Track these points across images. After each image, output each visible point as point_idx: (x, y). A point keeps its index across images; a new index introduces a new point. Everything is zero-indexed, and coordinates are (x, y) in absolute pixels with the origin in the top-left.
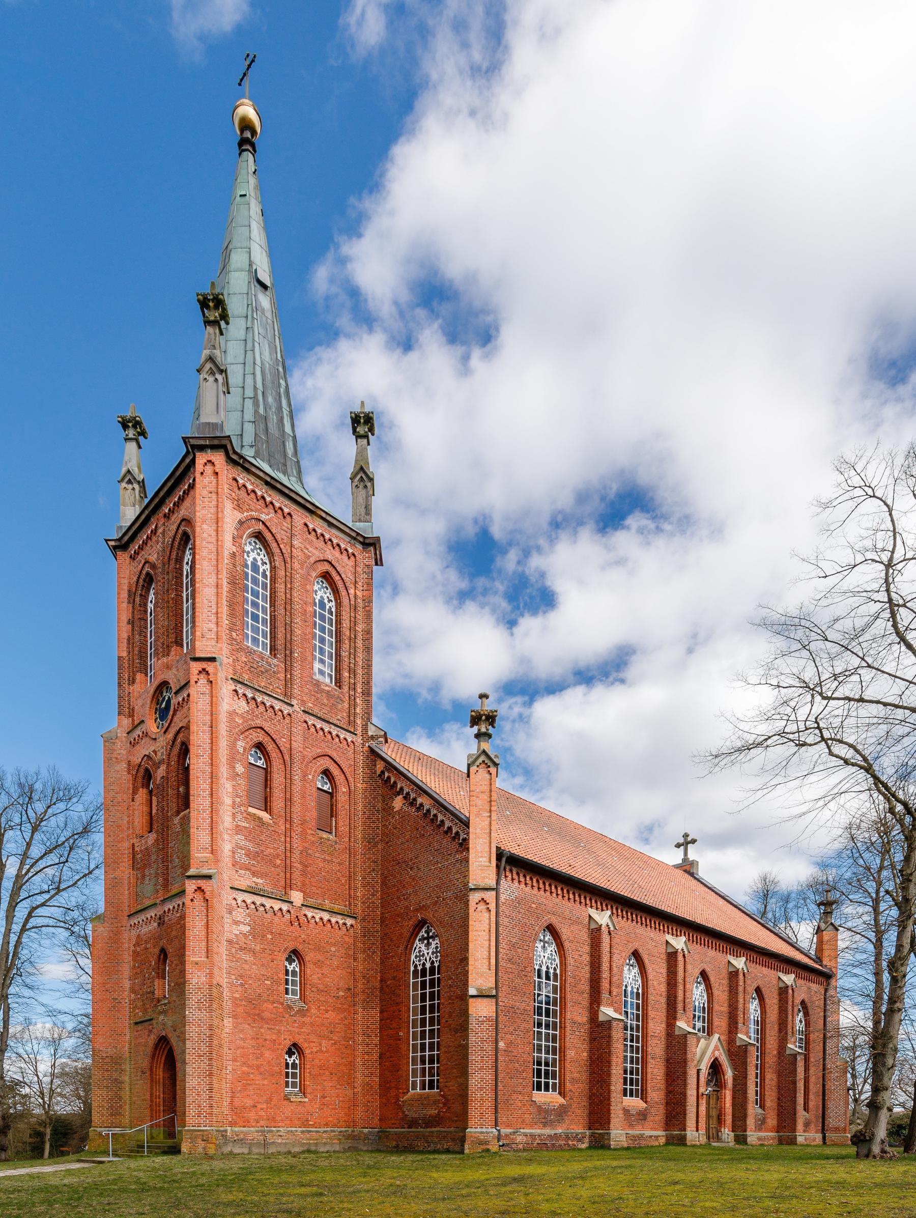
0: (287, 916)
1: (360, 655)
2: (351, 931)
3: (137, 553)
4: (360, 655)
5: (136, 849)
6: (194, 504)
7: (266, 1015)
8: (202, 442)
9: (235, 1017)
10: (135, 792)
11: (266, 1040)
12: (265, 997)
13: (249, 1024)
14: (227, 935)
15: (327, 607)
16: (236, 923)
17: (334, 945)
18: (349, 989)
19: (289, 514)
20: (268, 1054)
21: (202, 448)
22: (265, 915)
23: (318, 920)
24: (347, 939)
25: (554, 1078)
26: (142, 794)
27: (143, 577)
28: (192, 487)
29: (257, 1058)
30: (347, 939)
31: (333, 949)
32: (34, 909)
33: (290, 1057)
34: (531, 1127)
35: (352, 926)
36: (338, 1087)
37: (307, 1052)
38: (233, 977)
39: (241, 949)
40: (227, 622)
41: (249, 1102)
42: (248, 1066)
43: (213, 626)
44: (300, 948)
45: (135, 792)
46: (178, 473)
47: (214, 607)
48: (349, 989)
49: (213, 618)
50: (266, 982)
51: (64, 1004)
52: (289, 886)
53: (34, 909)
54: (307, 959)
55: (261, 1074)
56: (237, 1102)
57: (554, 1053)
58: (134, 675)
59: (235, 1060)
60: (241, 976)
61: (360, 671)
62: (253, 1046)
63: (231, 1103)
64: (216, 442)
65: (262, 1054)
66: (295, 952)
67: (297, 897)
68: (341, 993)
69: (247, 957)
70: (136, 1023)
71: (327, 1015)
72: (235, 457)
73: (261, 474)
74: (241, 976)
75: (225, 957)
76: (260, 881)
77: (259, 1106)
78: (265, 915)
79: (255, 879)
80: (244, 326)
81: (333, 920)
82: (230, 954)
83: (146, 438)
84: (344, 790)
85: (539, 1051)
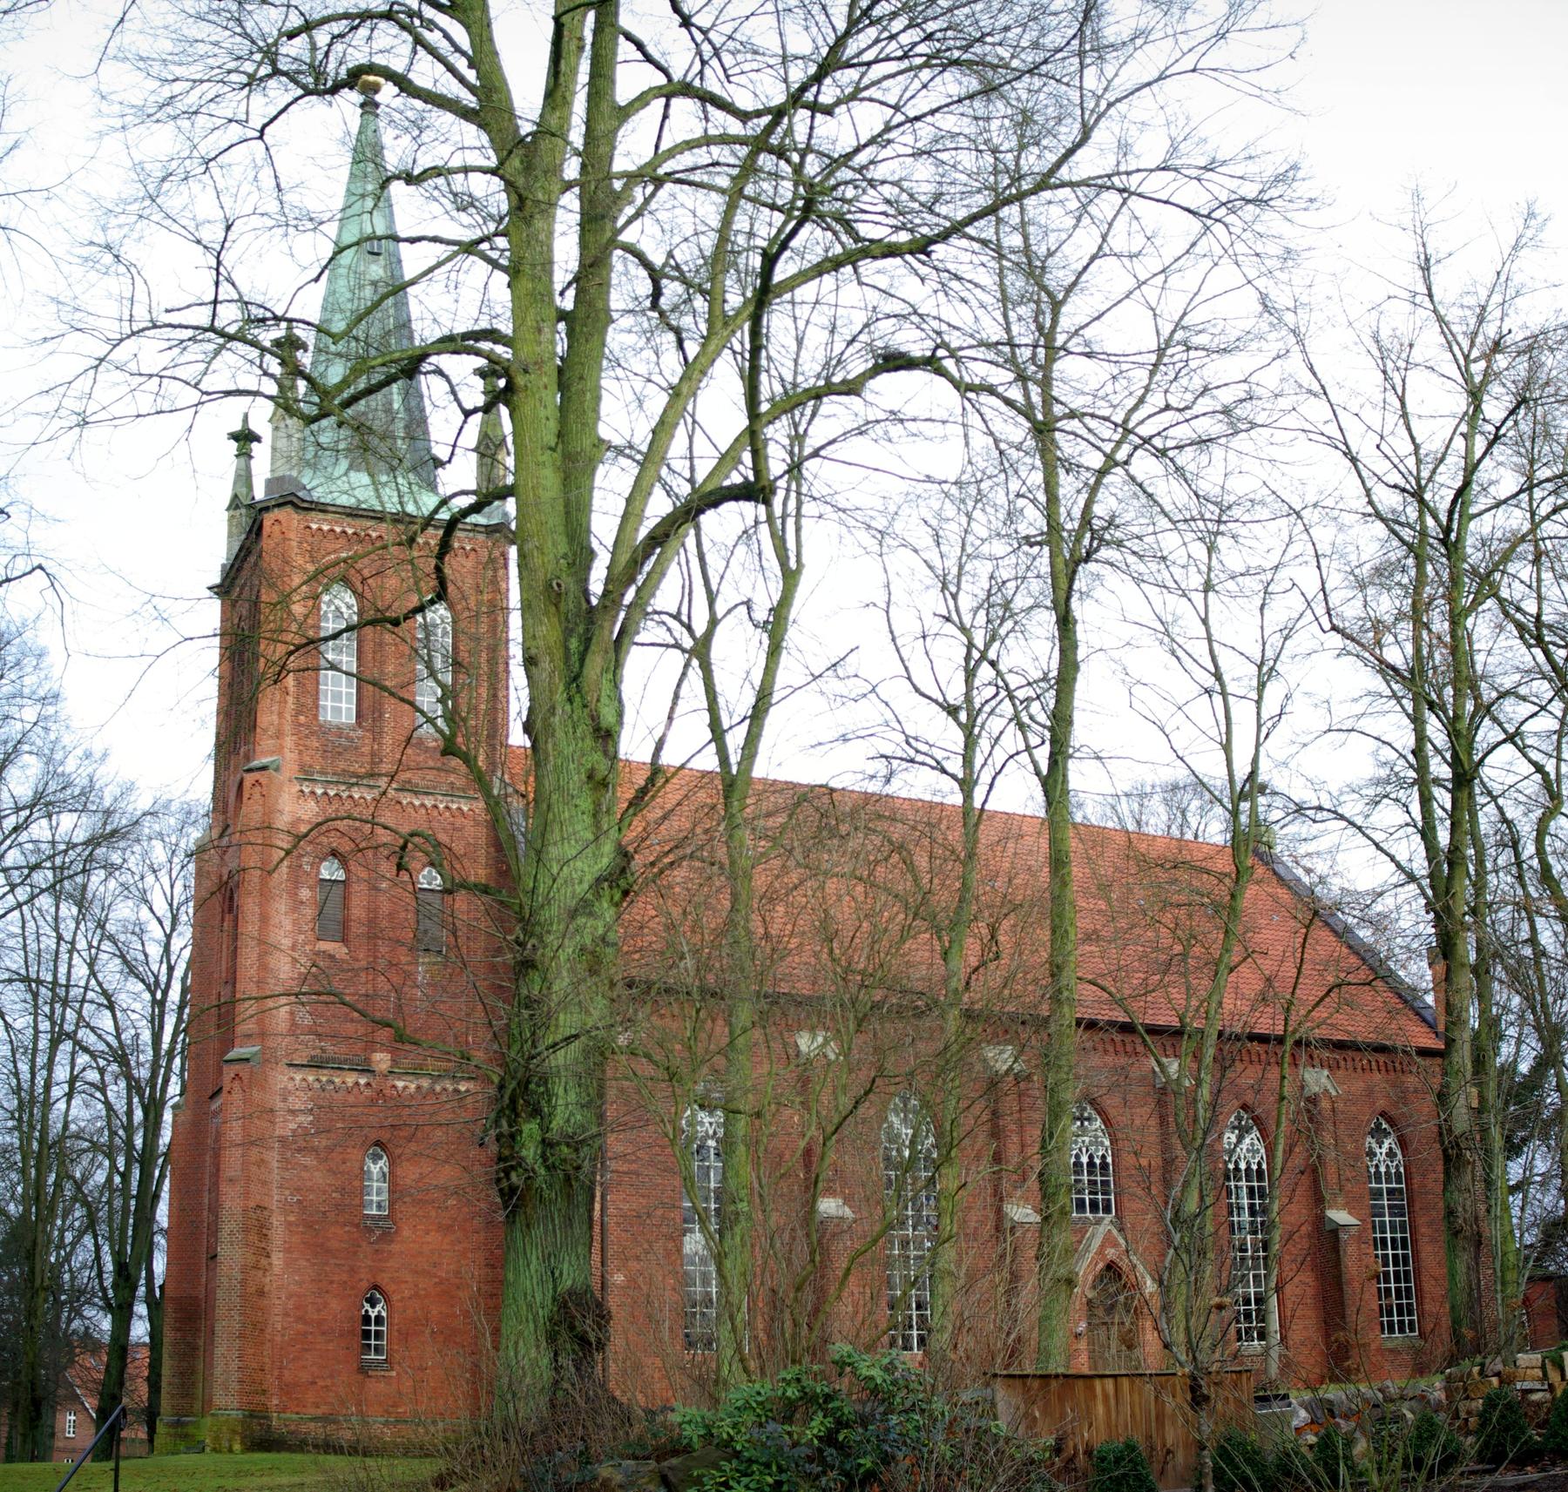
0: (368, 1092)
7: (334, 1244)
9: (288, 1251)
12: (332, 1216)
16: (293, 1112)
20: (335, 1305)
25: (1410, 1313)
32: (991, 390)
37: (395, 1298)
39: (299, 1150)
41: (304, 1377)
42: (306, 1323)
44: (385, 1136)
51: (820, 1040)
53: (991, 390)
56: (288, 1376)
57: (1404, 1247)
59: (286, 1315)
60: (298, 1190)
65: (326, 1305)
67: (381, 1060)
69: (308, 1160)
71: (428, 1239)
74: (298, 1190)
77: (321, 1383)
82: (284, 1160)
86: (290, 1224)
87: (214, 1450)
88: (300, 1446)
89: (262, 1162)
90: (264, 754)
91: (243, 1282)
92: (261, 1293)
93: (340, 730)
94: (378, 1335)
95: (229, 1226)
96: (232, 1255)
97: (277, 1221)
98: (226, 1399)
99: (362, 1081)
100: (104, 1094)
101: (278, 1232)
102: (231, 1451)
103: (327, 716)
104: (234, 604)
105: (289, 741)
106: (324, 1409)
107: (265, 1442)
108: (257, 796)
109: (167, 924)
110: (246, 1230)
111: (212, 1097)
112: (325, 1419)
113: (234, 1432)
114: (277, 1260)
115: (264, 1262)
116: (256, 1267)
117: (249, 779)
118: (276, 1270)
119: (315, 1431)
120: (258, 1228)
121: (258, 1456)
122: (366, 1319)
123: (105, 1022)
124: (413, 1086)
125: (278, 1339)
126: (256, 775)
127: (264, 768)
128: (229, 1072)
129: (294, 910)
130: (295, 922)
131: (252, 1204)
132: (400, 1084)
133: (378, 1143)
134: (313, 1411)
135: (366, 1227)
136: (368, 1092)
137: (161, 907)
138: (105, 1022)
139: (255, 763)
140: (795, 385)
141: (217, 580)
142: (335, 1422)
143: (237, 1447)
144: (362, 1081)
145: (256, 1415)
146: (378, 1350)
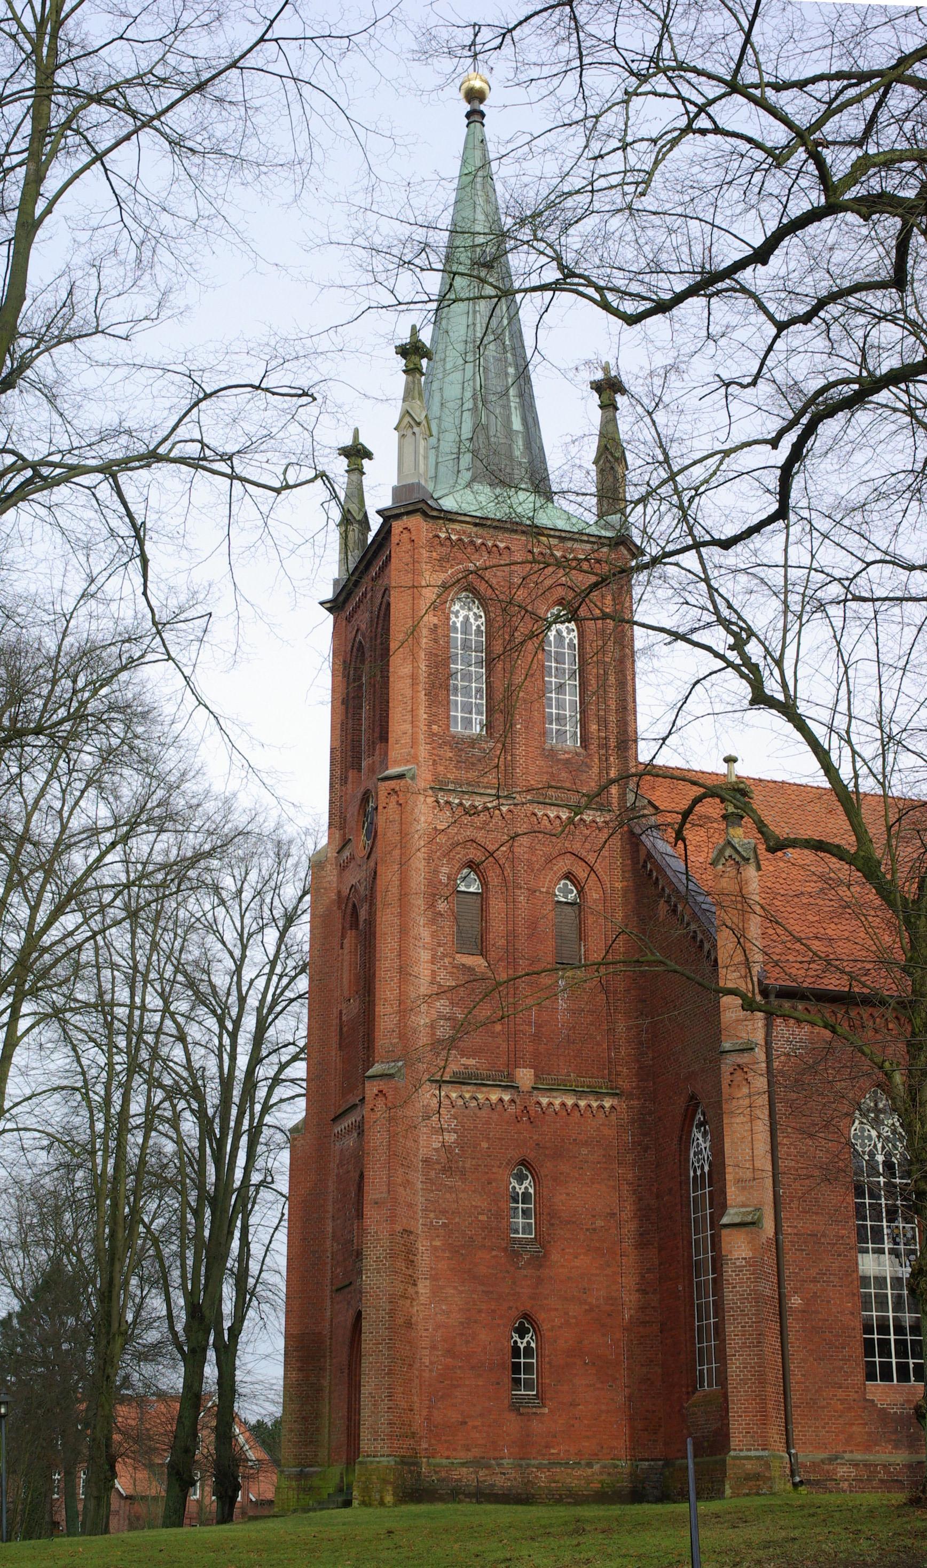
1: (612, 693)
2: (613, 1117)
3: (351, 616)
4: (612, 693)
5: (344, 1018)
6: (389, 577)
8: (397, 511)
9: (434, 1278)
10: (343, 936)
11: (480, 1311)
13: (455, 1288)
14: (423, 1152)
15: (567, 641)
17: (586, 1144)
18: (613, 1215)
19: (508, 548)
20: (484, 1336)
21: (398, 516)
22: (479, 1113)
23: (557, 1107)
24: (606, 1131)
26: (350, 937)
27: (356, 645)
28: (389, 558)
29: (467, 1342)
30: (606, 1131)
31: (584, 1151)
33: (522, 1337)
34: (868, 1448)
35: (612, 1107)
36: (599, 1386)
37: (545, 1327)
38: (432, 1215)
40: (425, 716)
43: (408, 727)
44: (531, 1156)
45: (343, 936)
46: (368, 556)
47: (409, 702)
48: (613, 1215)
49: (408, 717)
50: (480, 1217)
52: (514, 1062)
54: (543, 1172)
55: (473, 1368)
58: (347, 772)
59: (434, 1347)
60: (444, 1212)
61: (612, 718)
62: (461, 1323)
63: (428, 1418)
64: (411, 508)
66: (524, 1163)
67: (525, 1076)
68: (599, 1223)
70: (338, 1290)
71: (577, 1263)
72: (435, 513)
73: (468, 519)
75: (420, 1186)
76: (471, 1062)
78: (479, 1113)
79: (464, 1061)
80: (465, 323)
81: (582, 1103)
83: (371, 459)
84: (595, 896)
85: (882, 1305)
86: (435, 1248)
87: (364, 1503)
88: (455, 1494)
89: (407, 1183)
90: (397, 763)
91: (392, 1313)
92: (409, 1325)
93: (473, 742)
94: (528, 1368)
95: (375, 1252)
96: (376, 1281)
97: (422, 1246)
98: (378, 1450)
99: (506, 1098)
100: (176, 1128)
101: (424, 1260)
102: (382, 1503)
103: (458, 729)
104: (348, 619)
105: (423, 751)
106: (476, 1452)
107: (415, 1492)
108: (392, 805)
109: (237, 953)
110: (393, 1256)
111: (335, 1120)
112: (477, 1463)
113: (385, 1481)
114: (424, 1288)
115: (411, 1290)
116: (404, 1297)
117: (384, 787)
118: (423, 1299)
119: (466, 1476)
120: (406, 1254)
121: (414, 1508)
122: (516, 1351)
123: (178, 1053)
124: (557, 1102)
125: (426, 1375)
126: (392, 784)
127: (401, 776)
128: (371, 1089)
129: (433, 921)
130: (434, 935)
131: (399, 1228)
132: (545, 1101)
133: (524, 1163)
134: (463, 1456)
135: (513, 1251)
136: (512, 1109)
137: (230, 936)
138: (178, 1053)
139: (392, 771)
140: (100, 750)
141: (329, 594)
142: (488, 1467)
143: (389, 1499)
144: (506, 1098)
145: (409, 1462)
146: (529, 1385)
